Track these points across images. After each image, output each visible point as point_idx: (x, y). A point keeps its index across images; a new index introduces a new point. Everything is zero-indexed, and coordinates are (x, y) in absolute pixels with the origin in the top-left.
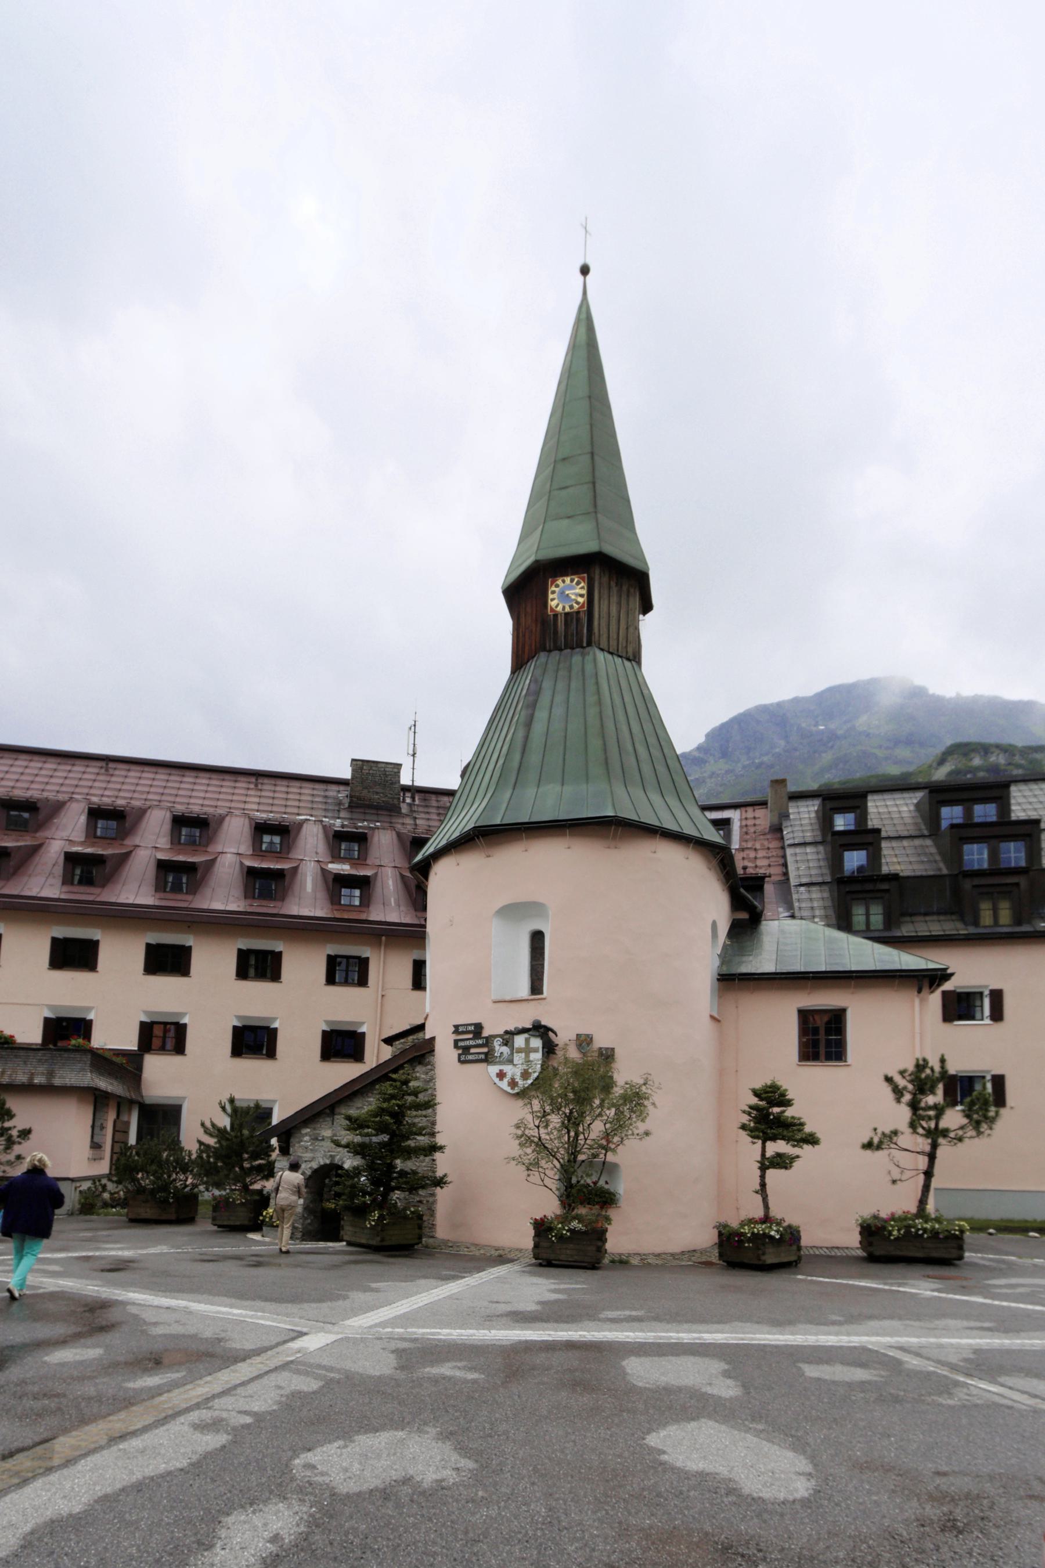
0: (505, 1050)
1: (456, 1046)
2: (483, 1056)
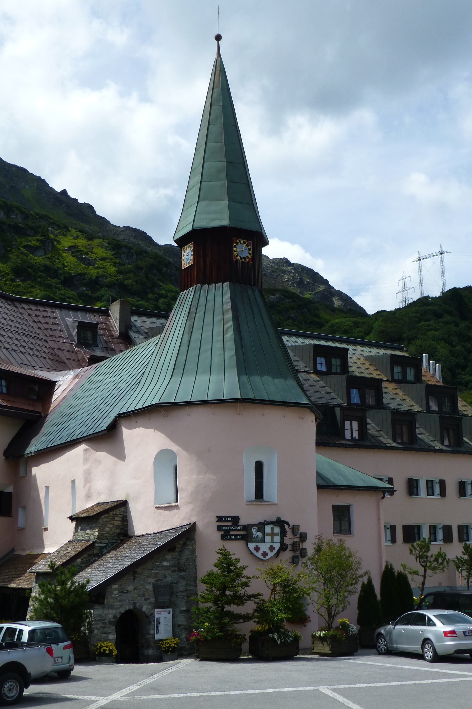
0: (259, 534)
1: (219, 528)
2: (241, 537)
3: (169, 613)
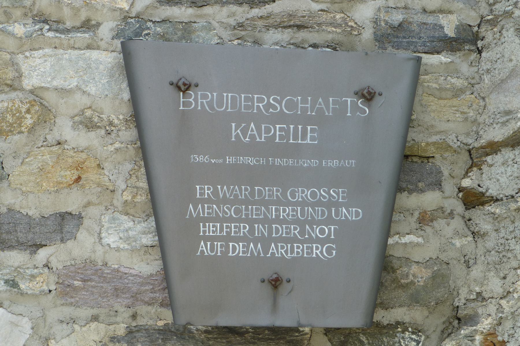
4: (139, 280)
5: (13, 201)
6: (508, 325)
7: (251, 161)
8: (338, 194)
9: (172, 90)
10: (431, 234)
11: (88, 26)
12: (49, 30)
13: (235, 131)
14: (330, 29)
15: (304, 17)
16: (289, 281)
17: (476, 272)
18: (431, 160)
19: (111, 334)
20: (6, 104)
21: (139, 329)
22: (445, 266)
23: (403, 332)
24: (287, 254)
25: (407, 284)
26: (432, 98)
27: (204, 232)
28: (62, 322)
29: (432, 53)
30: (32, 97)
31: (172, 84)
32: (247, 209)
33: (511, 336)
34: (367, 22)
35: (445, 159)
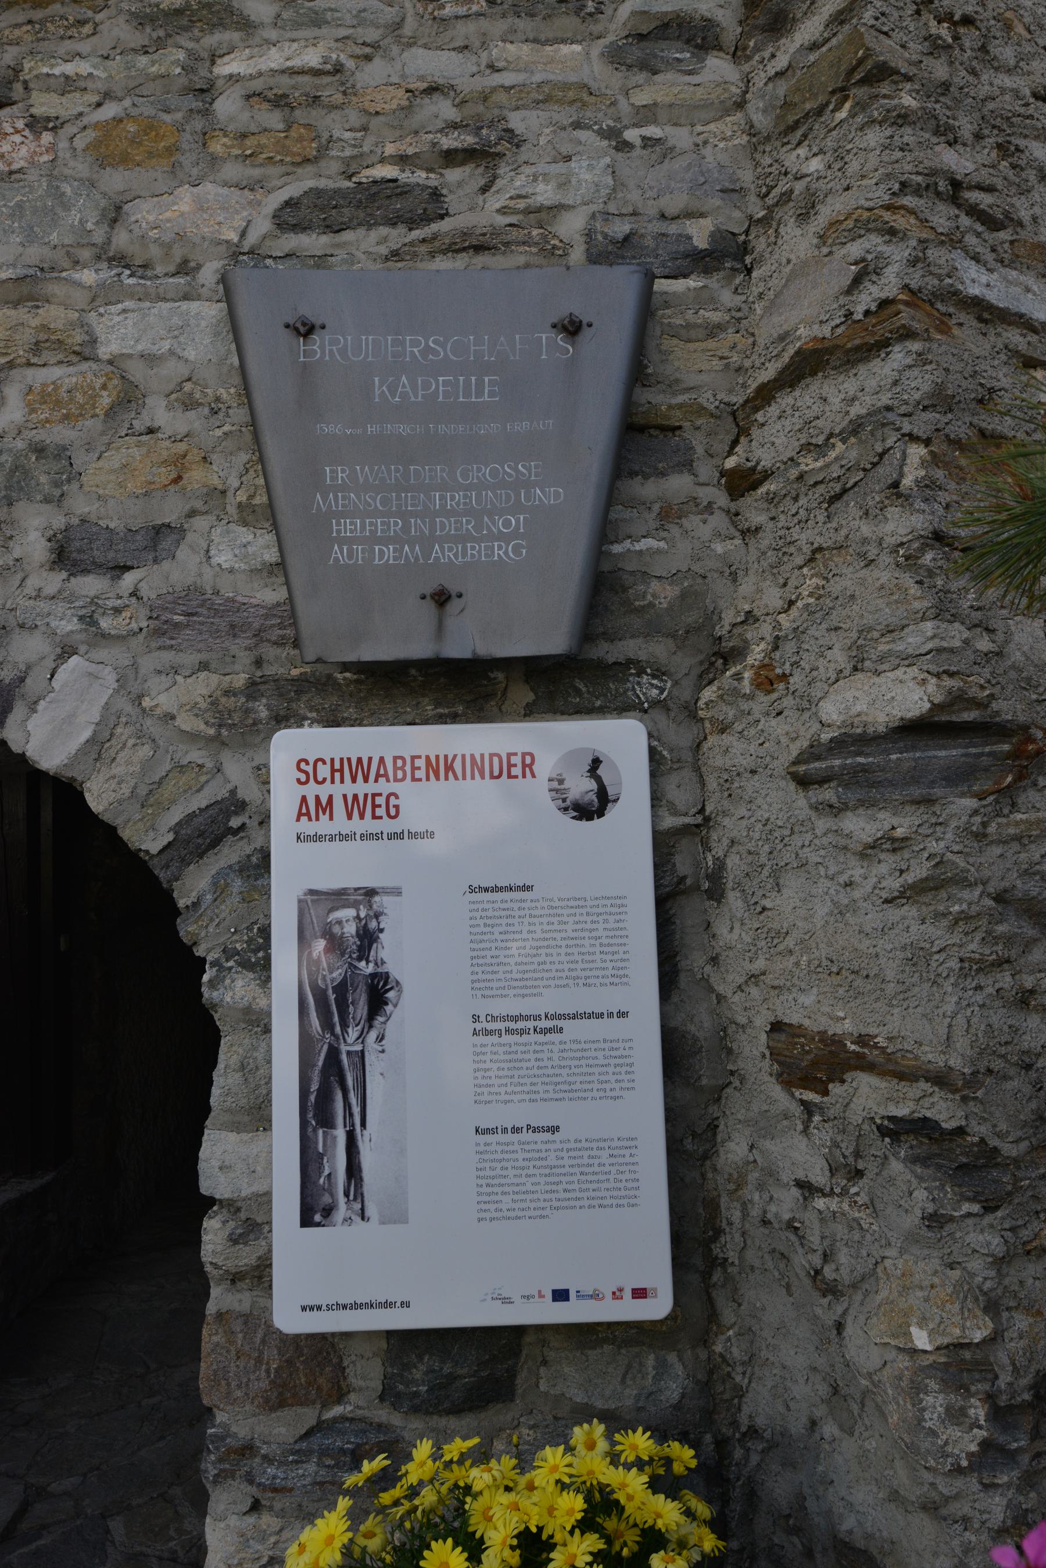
3: (591, 809)
4: (263, 611)
5: (87, 510)
6: (789, 647)
7: (404, 429)
8: (529, 470)
9: (286, 335)
10: (678, 535)
11: (184, 268)
12: (130, 276)
13: (379, 388)
14: (521, 249)
15: (484, 235)
16: (460, 596)
17: (747, 586)
18: (677, 433)
19: (225, 685)
20: (74, 380)
21: (265, 680)
22: (700, 581)
23: (639, 675)
24: (457, 558)
25: (643, 607)
26: (675, 341)
27: (339, 531)
28: (160, 672)
29: (675, 277)
30: (110, 368)
31: (287, 326)
32: (399, 498)
33: (795, 664)
34: (577, 237)
35: (698, 428)
